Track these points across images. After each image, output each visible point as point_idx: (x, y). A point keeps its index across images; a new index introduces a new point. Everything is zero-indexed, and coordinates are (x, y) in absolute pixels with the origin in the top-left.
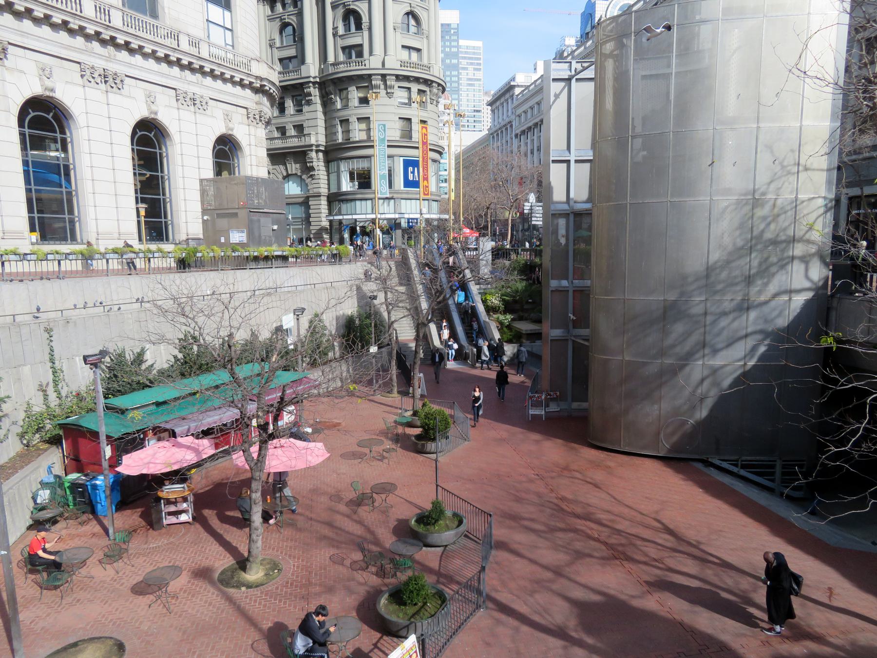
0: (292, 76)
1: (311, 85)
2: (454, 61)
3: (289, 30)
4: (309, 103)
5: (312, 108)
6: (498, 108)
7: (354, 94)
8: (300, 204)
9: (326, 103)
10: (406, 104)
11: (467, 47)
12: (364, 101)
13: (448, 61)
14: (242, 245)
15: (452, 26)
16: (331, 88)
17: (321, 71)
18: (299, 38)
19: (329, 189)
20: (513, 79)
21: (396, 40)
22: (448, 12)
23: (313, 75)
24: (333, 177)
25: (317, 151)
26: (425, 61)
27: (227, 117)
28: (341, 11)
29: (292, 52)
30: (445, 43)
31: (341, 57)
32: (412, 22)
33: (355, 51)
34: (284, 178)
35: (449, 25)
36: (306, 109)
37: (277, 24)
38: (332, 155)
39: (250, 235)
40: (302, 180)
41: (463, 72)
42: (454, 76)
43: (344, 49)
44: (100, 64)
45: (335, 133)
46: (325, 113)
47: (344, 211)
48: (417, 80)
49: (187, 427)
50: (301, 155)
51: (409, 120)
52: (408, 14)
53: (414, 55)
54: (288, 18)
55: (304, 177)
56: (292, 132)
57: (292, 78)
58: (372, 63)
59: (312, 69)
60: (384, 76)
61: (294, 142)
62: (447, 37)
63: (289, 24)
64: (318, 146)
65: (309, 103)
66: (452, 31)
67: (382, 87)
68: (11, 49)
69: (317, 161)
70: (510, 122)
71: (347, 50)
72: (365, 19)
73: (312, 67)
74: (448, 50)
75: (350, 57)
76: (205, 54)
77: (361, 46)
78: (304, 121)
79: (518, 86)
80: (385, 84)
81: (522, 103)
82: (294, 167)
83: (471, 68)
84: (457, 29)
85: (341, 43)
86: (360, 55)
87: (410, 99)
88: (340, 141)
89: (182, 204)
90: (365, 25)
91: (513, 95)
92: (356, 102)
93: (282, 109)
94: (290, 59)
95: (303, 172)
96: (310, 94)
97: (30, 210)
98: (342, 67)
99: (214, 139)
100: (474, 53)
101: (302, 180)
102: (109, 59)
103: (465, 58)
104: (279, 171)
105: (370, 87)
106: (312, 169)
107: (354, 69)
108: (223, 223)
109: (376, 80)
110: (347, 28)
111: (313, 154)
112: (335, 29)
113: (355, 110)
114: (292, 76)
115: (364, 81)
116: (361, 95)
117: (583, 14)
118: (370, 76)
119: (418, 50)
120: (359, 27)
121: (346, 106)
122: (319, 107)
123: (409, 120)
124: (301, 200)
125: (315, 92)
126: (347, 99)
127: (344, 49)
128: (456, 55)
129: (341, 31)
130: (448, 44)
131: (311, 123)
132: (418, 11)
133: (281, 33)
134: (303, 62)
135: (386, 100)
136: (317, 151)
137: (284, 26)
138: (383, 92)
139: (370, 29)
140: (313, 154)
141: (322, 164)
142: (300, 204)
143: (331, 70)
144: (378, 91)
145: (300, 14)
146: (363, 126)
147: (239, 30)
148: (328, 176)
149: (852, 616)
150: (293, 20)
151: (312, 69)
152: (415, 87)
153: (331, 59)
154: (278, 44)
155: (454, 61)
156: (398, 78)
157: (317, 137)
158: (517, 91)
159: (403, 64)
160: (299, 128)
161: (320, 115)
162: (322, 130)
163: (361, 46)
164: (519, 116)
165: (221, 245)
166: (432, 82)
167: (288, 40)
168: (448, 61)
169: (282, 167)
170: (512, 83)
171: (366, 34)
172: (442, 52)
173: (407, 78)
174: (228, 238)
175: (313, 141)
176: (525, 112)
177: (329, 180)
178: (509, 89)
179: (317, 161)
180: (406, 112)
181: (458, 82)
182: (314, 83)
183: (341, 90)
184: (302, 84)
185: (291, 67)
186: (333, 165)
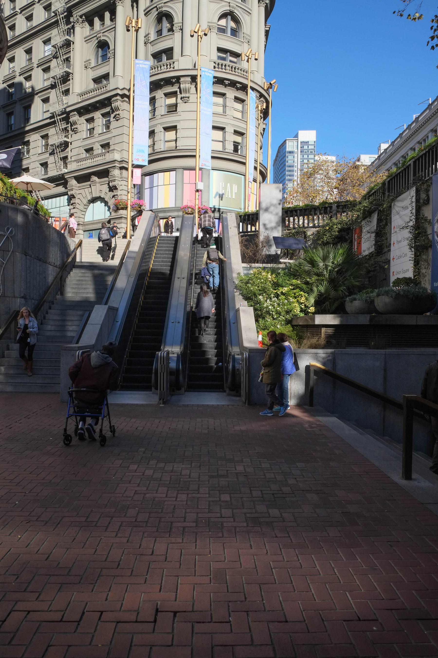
1: (118, 97)
12: (173, 109)
15: (310, 143)
30: (303, 156)
48: (233, 84)
49: (354, 532)
54: (103, 36)
56: (98, 150)
72: (177, 19)
78: (110, 138)
104: (84, 196)
109: (185, 82)
118: (178, 78)
129: (153, 37)
131: (118, 140)
132: (238, 13)
144: (187, 95)
149: (85, 328)
170: (358, 163)
185: (190, 210)
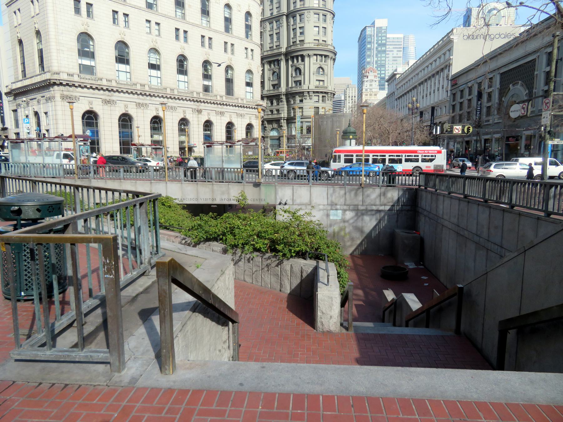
0: (276, 91)
2: (383, 48)
3: (276, 74)
4: (282, 101)
5: (282, 103)
6: (390, 84)
7: (298, 99)
8: (277, 139)
9: (288, 102)
10: (317, 101)
11: (393, 38)
12: (301, 101)
13: (379, 49)
14: (251, 155)
15: (383, 28)
16: (289, 96)
17: (286, 90)
18: (279, 78)
19: (288, 133)
20: (396, 70)
21: (314, 78)
22: (381, 20)
23: (283, 91)
24: (290, 129)
25: (284, 120)
26: (326, 85)
27: (250, 118)
28: (294, 68)
29: (276, 82)
30: (378, 38)
31: (294, 85)
32: (321, 70)
33: (298, 83)
34: (272, 129)
35: (381, 28)
36: (280, 103)
37: (272, 72)
38: (290, 121)
39: (253, 153)
40: (278, 130)
41: (391, 53)
42: (383, 57)
43: (295, 82)
44: (220, 110)
45: (291, 113)
46: (287, 105)
47: (292, 142)
48: (322, 92)
50: (278, 121)
51: (318, 108)
52: (319, 68)
53: (321, 83)
55: (279, 129)
56: (275, 112)
57: (275, 92)
58: (305, 87)
59: (283, 89)
60: (308, 92)
61: (275, 116)
62: (380, 35)
63: (276, 72)
64: (284, 118)
65: (282, 101)
66: (383, 31)
67: (308, 96)
68: (203, 110)
69: (284, 123)
70: (394, 92)
71: (296, 82)
72: (302, 71)
73: (283, 89)
74: (380, 42)
75: (297, 85)
76: (245, 102)
77: (301, 80)
79: (398, 74)
80: (309, 95)
81: (398, 83)
82: (275, 126)
83: (395, 50)
84: (386, 29)
85: (294, 79)
86: (300, 84)
87: (319, 100)
88: (292, 116)
89: (216, 137)
90: (302, 73)
91: (395, 79)
92: (298, 102)
93: (272, 103)
94: (276, 85)
95: (278, 127)
96: (282, 98)
97: (120, 145)
98: (294, 89)
99: (246, 125)
100: (398, 42)
101: (278, 130)
102: (222, 108)
103: (391, 45)
105: (303, 96)
106: (282, 126)
107: (298, 89)
108: (247, 150)
110: (296, 74)
111: (282, 121)
112: (292, 74)
113: (298, 104)
114: (276, 91)
115: (301, 94)
116: (300, 99)
117: (464, 16)
119: (323, 81)
120: (300, 74)
121: (295, 103)
122: (285, 103)
123: (318, 108)
124: (277, 138)
125: (284, 97)
126: (295, 100)
127: (295, 82)
128: (385, 45)
129: (294, 75)
130: (380, 38)
131: (282, 109)
133: (273, 75)
134: (280, 86)
135: (309, 101)
136: (284, 120)
137: (274, 73)
138: (308, 98)
139: (304, 75)
140: (282, 121)
141: (285, 124)
142: (277, 139)
143: (290, 90)
145: (280, 69)
146: (301, 110)
147: (254, 93)
148: (288, 129)
150: (277, 70)
151: (283, 89)
152: (321, 95)
153: (290, 86)
154: (272, 79)
155: (383, 48)
156: (314, 92)
157: (284, 114)
158: (398, 76)
159: (316, 87)
160: (278, 110)
161: (286, 106)
162: (286, 111)
163: (301, 80)
164: (398, 89)
165: (246, 155)
166: (328, 92)
167: (275, 78)
168: (379, 49)
169: (271, 125)
170: (395, 73)
171: (303, 76)
172: (376, 43)
173: (317, 92)
174: (248, 154)
175: (282, 116)
176: (400, 88)
177: (288, 130)
178: (394, 75)
179: (284, 123)
180: (317, 105)
181: (385, 60)
182: (284, 94)
183: (293, 97)
184: (279, 95)
186: (289, 125)
